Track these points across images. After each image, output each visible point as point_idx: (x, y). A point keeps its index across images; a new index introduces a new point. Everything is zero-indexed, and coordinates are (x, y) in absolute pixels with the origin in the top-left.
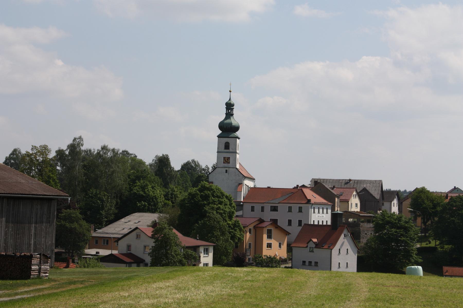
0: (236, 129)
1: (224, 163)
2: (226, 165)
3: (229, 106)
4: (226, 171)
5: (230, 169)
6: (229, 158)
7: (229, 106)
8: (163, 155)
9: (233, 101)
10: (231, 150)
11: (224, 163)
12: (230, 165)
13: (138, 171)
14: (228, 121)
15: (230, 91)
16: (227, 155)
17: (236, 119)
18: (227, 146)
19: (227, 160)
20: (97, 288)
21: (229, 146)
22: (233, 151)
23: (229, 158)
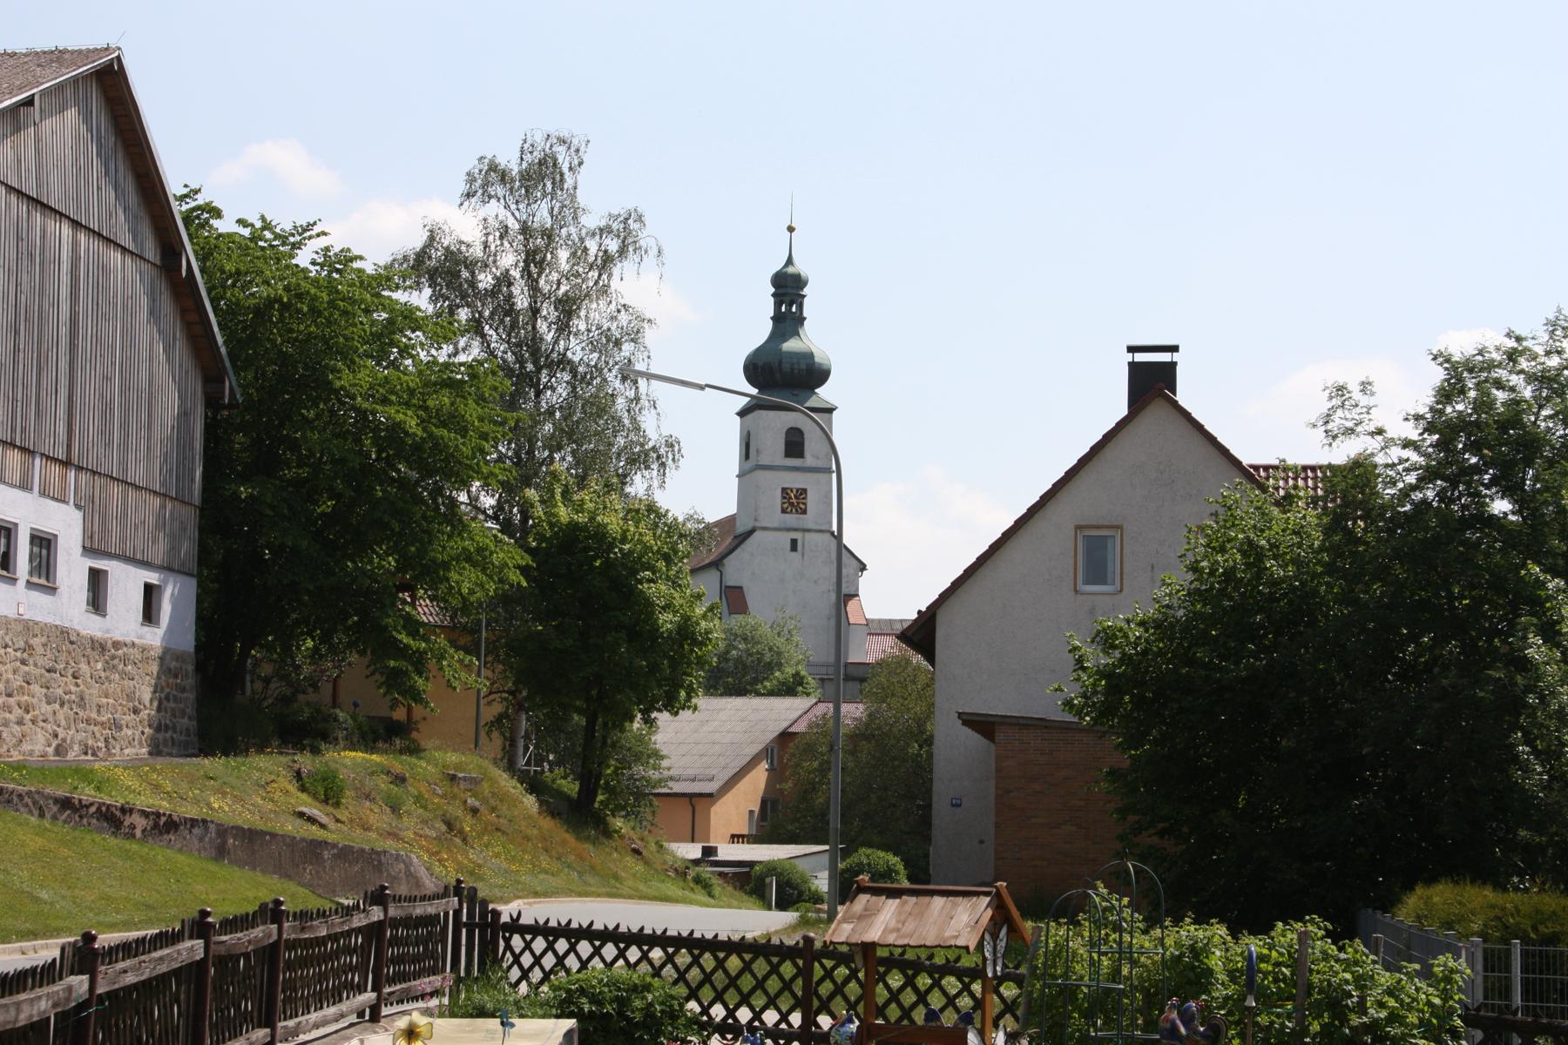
0: (818, 375)
1: (784, 511)
2: (792, 519)
3: (788, 288)
4: (794, 543)
5: (807, 535)
6: (805, 491)
7: (788, 288)
8: (625, 235)
9: (801, 266)
10: (809, 460)
11: (784, 511)
12: (809, 520)
13: (847, 678)
14: (791, 345)
15: (791, 229)
16: (795, 481)
17: (818, 336)
18: (794, 444)
19: (794, 501)
20: (657, 590)
21: (802, 444)
22: (820, 464)
23: (805, 491)
